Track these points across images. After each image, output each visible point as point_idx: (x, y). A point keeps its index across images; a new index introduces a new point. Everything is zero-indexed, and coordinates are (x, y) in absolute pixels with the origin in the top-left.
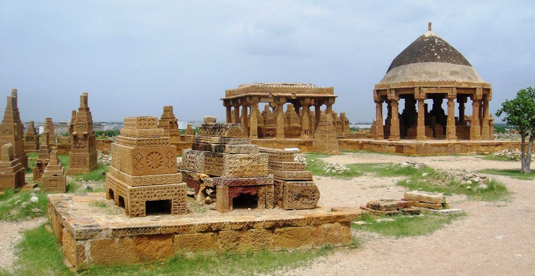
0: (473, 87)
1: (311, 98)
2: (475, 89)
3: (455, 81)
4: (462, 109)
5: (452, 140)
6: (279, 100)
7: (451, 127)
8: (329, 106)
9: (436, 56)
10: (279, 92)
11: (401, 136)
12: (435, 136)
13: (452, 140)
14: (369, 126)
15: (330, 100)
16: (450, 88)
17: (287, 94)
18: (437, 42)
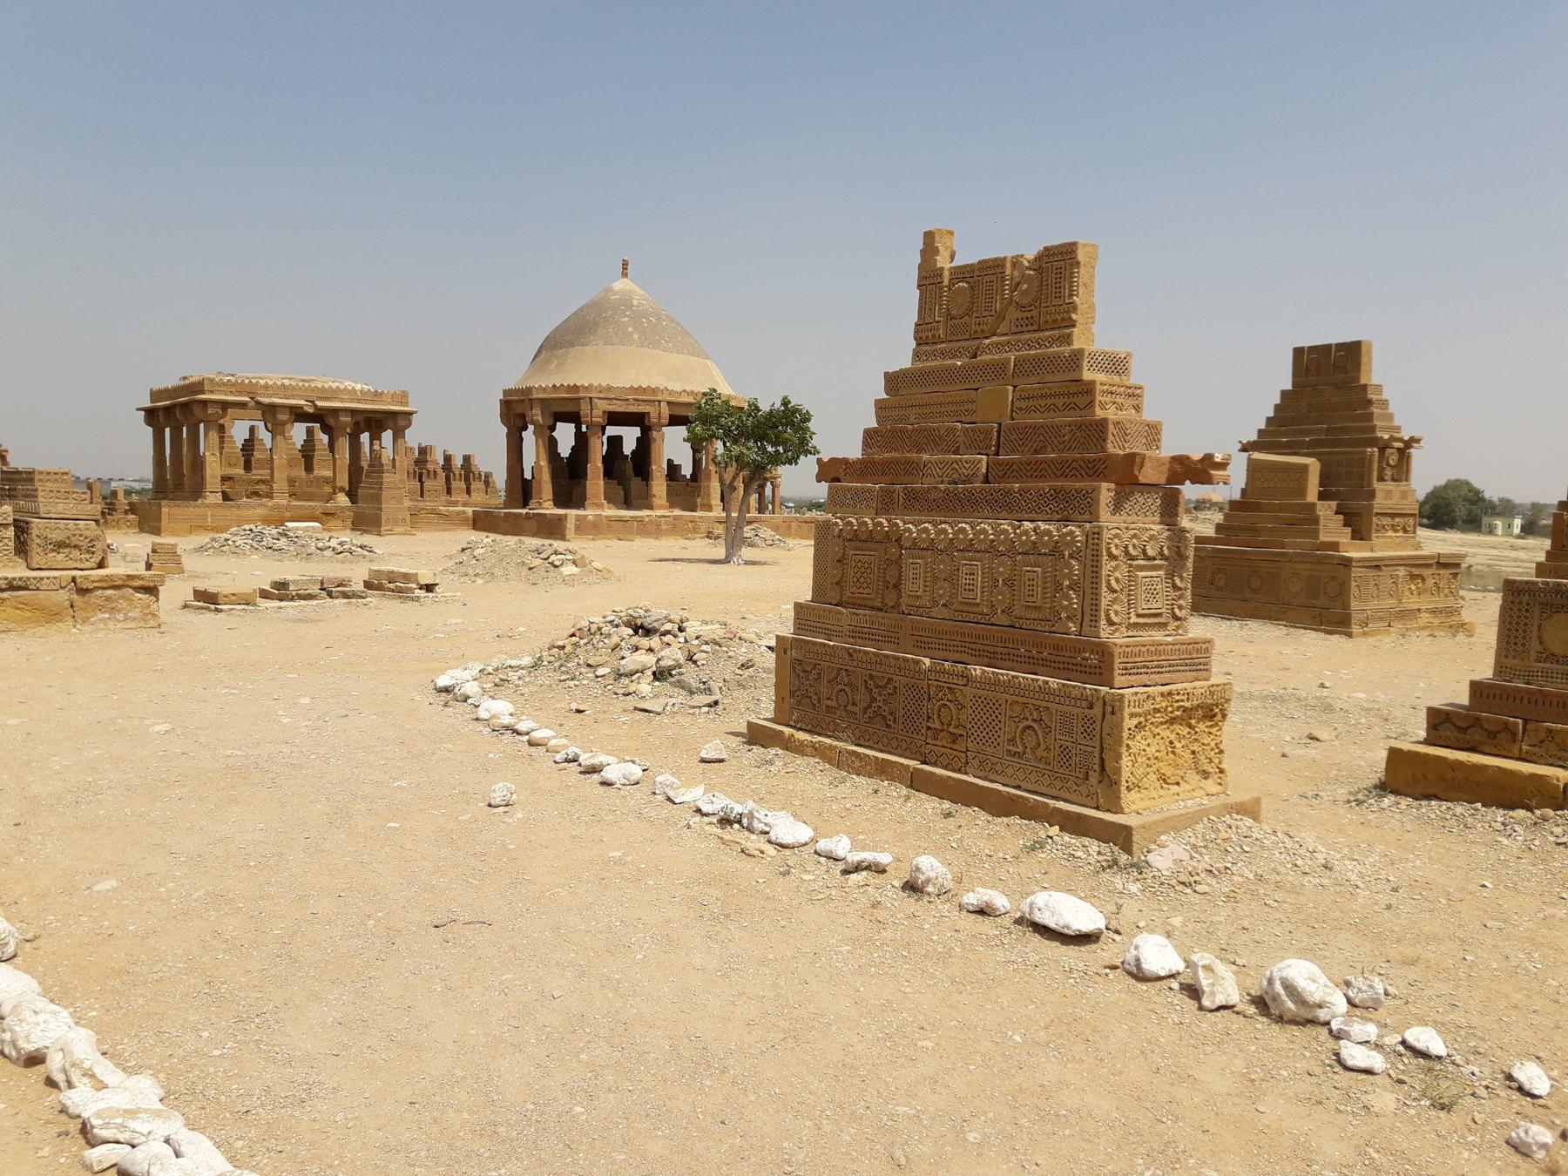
1: (353, 412)
5: (662, 511)
6: (274, 415)
7: (659, 486)
8: (399, 434)
10: (274, 395)
12: (628, 504)
13: (662, 511)
14: (746, 553)
15: (401, 423)
17: (293, 402)
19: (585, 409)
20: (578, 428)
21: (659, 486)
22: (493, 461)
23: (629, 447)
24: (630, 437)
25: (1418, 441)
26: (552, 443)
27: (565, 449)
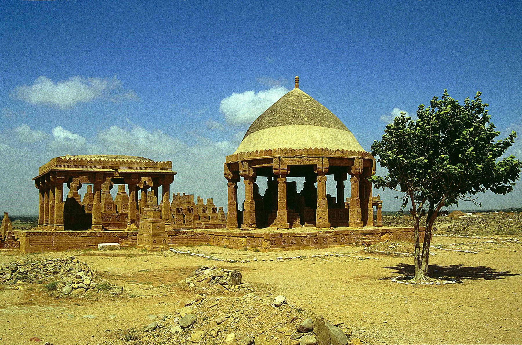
0: (350, 156)
2: (353, 159)
3: (327, 149)
4: (340, 188)
5: (322, 227)
7: (322, 212)
9: (303, 118)
11: (257, 224)
16: (320, 157)
18: (304, 100)
19: (275, 164)
20: (270, 179)
21: (322, 212)
22: (222, 201)
23: (300, 188)
24: (300, 182)
25: (176, 173)
26: (256, 188)
27: (262, 192)
